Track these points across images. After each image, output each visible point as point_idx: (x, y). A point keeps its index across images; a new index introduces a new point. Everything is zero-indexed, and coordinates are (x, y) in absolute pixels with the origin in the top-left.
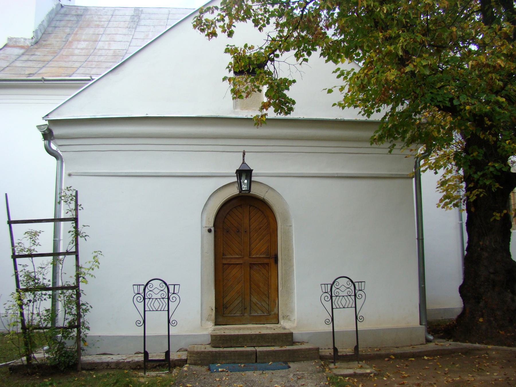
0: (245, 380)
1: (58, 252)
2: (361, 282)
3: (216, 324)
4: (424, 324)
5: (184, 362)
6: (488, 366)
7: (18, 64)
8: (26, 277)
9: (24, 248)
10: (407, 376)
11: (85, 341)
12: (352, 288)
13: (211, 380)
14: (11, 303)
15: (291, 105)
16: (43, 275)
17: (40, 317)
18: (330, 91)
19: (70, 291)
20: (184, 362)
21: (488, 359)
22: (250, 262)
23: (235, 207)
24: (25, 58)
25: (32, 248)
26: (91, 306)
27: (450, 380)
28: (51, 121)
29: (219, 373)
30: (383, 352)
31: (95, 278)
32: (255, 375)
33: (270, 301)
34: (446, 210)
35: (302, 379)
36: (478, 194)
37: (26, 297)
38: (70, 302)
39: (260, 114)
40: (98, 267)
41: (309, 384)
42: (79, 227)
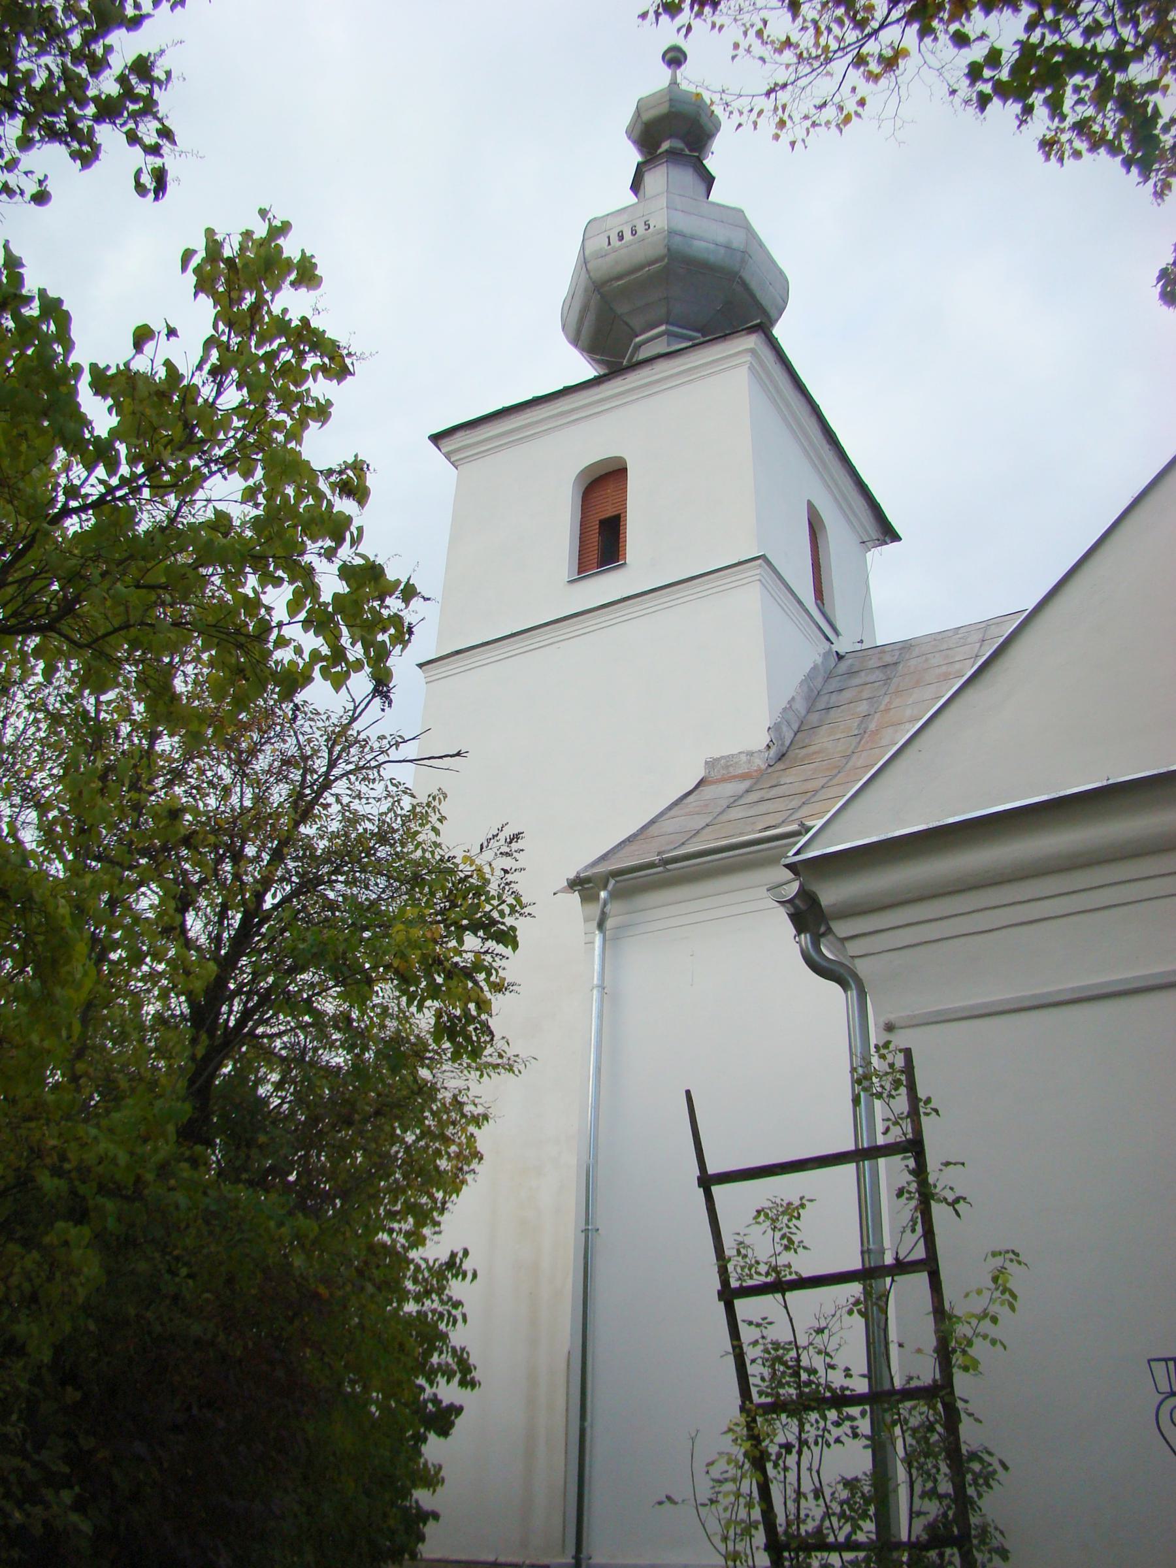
7: (735, 813)
24: (754, 797)
25: (782, 1260)
31: (1005, 1348)
37: (771, 1436)
40: (1012, 1308)
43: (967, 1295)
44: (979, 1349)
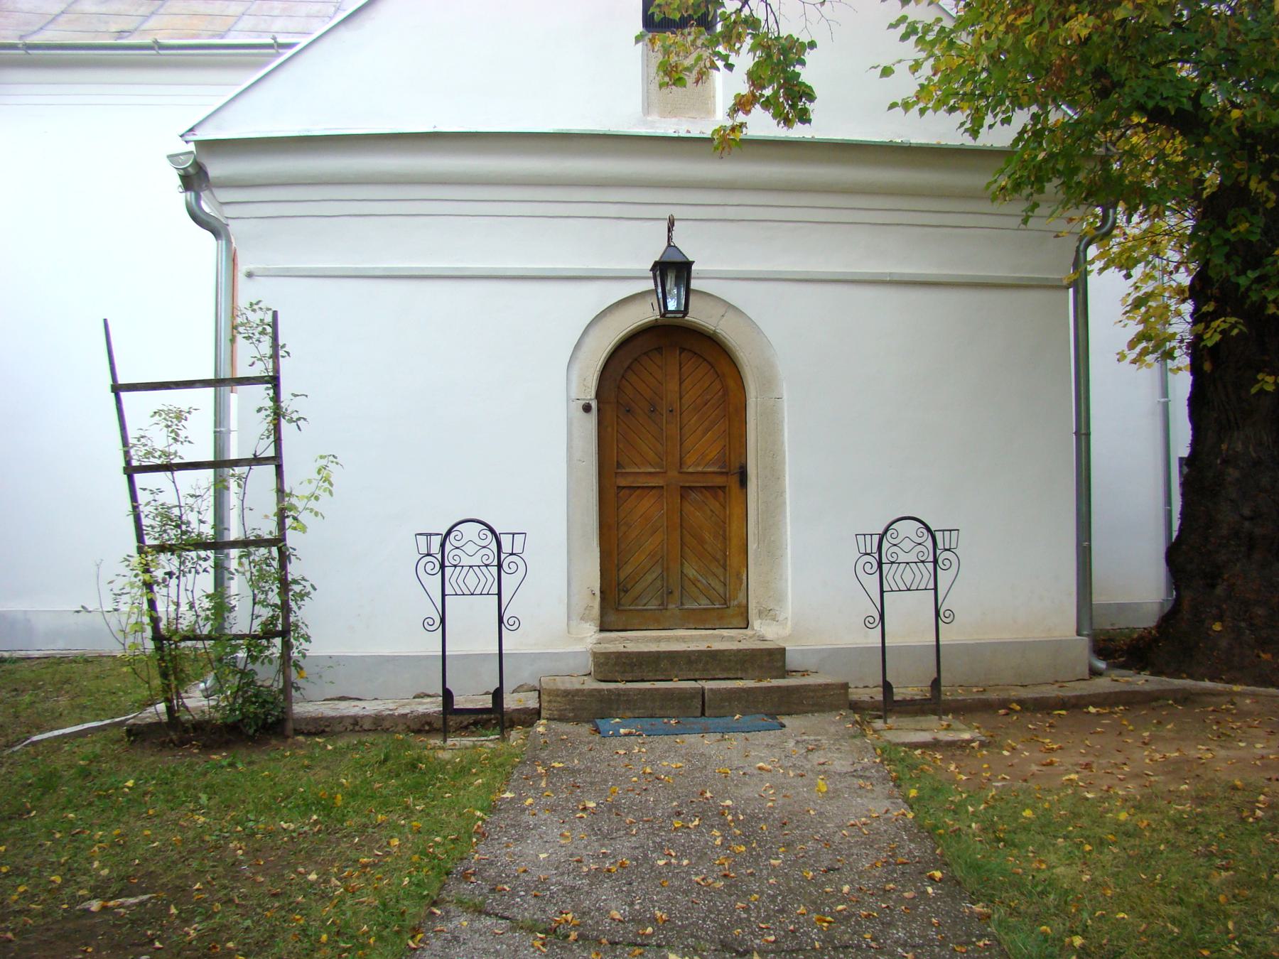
0: (687, 754)
1: (226, 458)
2: (950, 531)
3: (602, 630)
4: (1085, 633)
5: (532, 714)
6: (1240, 728)
8: (158, 519)
9: (153, 449)
10: (1057, 749)
11: (301, 668)
12: (929, 543)
13: (605, 754)
14: (126, 580)
15: (805, 103)
16: (199, 512)
17: (196, 611)
18: (886, 72)
19: (263, 551)
20: (532, 714)
21: (1236, 714)
22: (682, 484)
23: (645, 353)
25: (172, 450)
26: (312, 586)
27: (1157, 756)
28: (201, 144)
29: (620, 739)
30: (993, 695)
32: (706, 742)
33: (728, 575)
34: (1138, 369)
35: (818, 750)
36: (1224, 329)
38: (262, 576)
39: (729, 123)
41: (835, 763)
42: (282, 399)
43: (301, 483)
44: (305, 517)
